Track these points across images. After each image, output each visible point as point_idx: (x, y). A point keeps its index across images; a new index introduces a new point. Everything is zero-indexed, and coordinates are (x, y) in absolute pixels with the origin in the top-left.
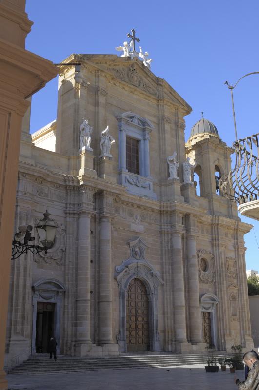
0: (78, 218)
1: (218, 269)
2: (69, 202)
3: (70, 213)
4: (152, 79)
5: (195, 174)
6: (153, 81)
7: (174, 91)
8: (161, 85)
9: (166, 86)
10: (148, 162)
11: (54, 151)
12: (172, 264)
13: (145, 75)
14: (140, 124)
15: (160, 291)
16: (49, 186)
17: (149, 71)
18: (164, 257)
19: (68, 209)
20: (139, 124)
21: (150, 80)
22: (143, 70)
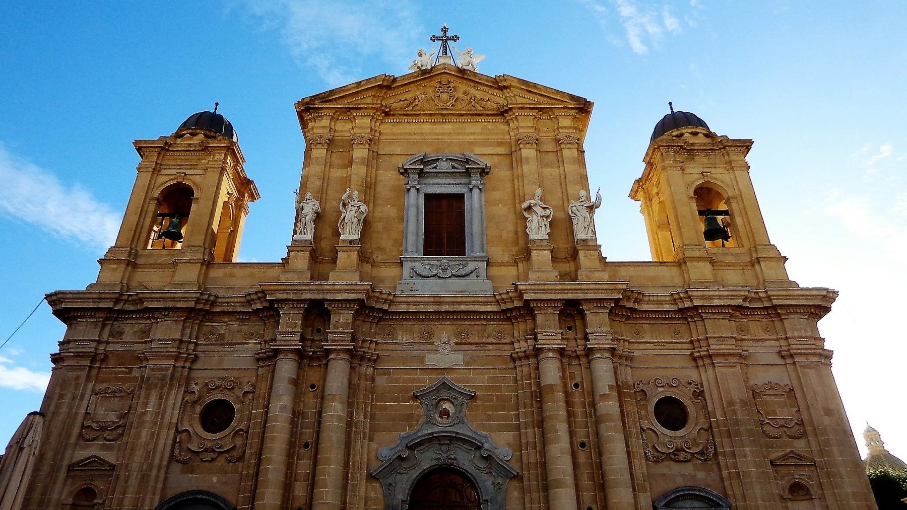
0: (589, 362)
1: (719, 417)
2: (695, 338)
3: (701, 357)
4: (487, 86)
5: (216, 233)
6: (491, 87)
7: (535, 85)
8: (505, 87)
9: (513, 84)
10: (476, 228)
11: (646, 255)
12: (541, 424)
13: (472, 84)
14: (456, 165)
15: (516, 494)
16: (226, 320)
17: (475, 74)
18: (522, 410)
19: (697, 349)
20: (453, 167)
21: (485, 88)
22: (463, 78)
